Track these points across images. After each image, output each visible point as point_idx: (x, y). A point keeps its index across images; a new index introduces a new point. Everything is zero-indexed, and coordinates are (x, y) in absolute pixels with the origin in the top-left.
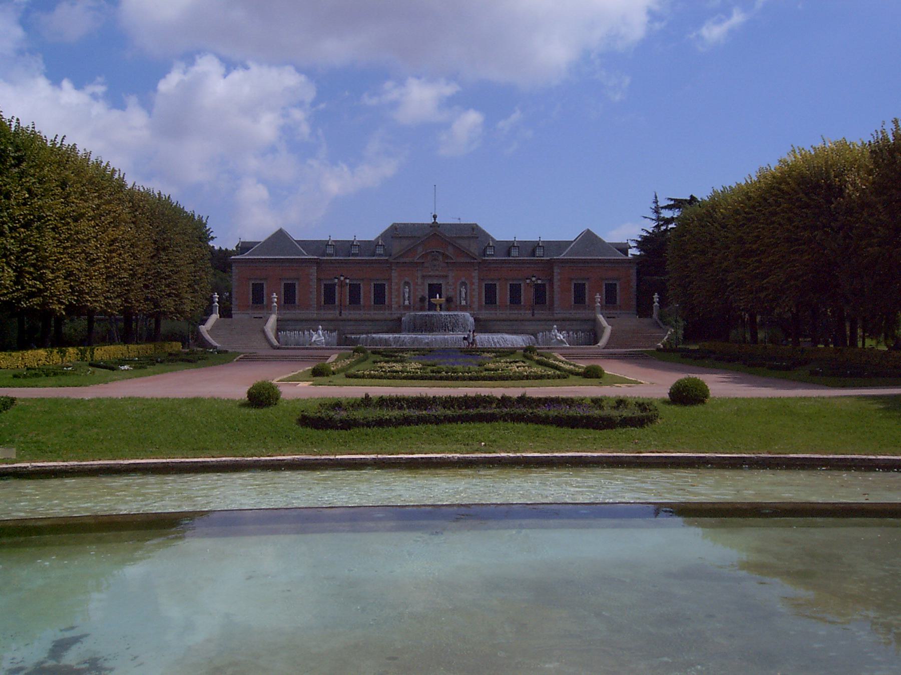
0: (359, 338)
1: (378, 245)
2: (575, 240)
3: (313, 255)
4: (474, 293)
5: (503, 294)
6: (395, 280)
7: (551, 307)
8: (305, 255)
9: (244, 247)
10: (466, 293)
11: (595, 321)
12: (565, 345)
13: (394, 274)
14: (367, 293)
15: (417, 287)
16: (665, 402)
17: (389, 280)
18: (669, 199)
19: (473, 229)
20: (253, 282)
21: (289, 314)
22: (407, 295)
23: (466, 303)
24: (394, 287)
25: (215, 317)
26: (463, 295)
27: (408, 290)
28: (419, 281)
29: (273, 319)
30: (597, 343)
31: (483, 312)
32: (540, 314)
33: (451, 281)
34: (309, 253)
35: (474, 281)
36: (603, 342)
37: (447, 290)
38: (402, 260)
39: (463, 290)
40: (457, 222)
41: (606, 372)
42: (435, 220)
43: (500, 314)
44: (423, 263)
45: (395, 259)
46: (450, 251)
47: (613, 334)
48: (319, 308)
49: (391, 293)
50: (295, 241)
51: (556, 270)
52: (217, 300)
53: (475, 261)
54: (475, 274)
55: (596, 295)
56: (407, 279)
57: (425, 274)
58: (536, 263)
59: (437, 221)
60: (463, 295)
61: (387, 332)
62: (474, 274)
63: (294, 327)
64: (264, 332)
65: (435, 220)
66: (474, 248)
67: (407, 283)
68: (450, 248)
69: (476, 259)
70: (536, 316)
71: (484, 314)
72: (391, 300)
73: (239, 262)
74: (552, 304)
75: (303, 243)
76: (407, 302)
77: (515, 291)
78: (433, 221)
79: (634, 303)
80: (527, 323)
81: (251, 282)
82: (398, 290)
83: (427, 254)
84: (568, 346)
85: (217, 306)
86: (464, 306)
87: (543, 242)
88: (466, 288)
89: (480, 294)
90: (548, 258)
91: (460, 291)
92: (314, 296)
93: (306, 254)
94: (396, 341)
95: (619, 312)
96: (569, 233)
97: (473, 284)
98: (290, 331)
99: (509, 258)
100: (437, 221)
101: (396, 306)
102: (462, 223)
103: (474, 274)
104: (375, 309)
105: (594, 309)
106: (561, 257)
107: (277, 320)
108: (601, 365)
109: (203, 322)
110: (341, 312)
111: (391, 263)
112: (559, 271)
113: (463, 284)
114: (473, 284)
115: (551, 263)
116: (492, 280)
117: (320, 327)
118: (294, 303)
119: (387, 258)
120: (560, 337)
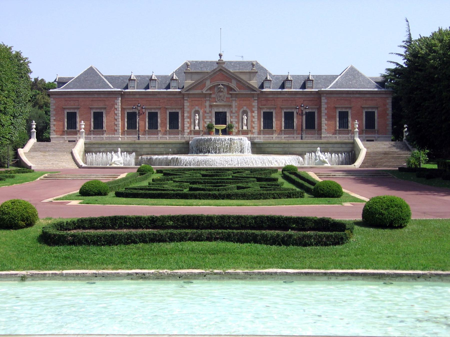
0: (151, 158)
1: (172, 79)
2: (340, 75)
3: (118, 88)
6: (187, 109)
8: (111, 88)
9: (61, 82)
10: (247, 120)
11: (354, 144)
12: (326, 165)
13: (187, 104)
15: (206, 115)
16: (358, 223)
17: (183, 109)
19: (253, 65)
21: (94, 138)
22: (197, 122)
23: (247, 128)
25: (33, 141)
26: (245, 122)
27: (197, 117)
28: (208, 110)
29: (81, 143)
30: (354, 163)
32: (309, 138)
36: (358, 164)
38: (191, 92)
39: (245, 117)
40: (240, 59)
41: (344, 190)
42: (221, 58)
43: (275, 138)
44: (211, 94)
46: (233, 85)
47: (367, 154)
48: (281, 132)
51: (324, 100)
52: (357, 126)
53: (255, 92)
54: (255, 104)
55: (33, 122)
59: (222, 59)
60: (245, 122)
62: (254, 104)
63: (99, 149)
64: (72, 153)
65: (221, 58)
66: (255, 83)
68: (234, 82)
69: (256, 91)
70: (305, 141)
71: (261, 139)
73: (71, 94)
74: (320, 129)
75: (112, 79)
76: (197, 128)
77: (153, 117)
79: (390, 128)
80: (297, 146)
83: (214, 87)
85: (34, 132)
86: (245, 130)
87: (293, 76)
88: (247, 116)
90: (317, 90)
91: (242, 119)
93: (112, 87)
95: (376, 135)
98: (96, 153)
100: (222, 59)
101: (189, 131)
103: (254, 104)
105: (353, 133)
106: (328, 89)
107: (85, 144)
108: (27, 199)
109: (23, 146)
110: (139, 137)
111: (183, 95)
112: (326, 101)
115: (319, 94)
116: (270, 108)
117: (119, 149)
119: (180, 90)
120: (322, 157)
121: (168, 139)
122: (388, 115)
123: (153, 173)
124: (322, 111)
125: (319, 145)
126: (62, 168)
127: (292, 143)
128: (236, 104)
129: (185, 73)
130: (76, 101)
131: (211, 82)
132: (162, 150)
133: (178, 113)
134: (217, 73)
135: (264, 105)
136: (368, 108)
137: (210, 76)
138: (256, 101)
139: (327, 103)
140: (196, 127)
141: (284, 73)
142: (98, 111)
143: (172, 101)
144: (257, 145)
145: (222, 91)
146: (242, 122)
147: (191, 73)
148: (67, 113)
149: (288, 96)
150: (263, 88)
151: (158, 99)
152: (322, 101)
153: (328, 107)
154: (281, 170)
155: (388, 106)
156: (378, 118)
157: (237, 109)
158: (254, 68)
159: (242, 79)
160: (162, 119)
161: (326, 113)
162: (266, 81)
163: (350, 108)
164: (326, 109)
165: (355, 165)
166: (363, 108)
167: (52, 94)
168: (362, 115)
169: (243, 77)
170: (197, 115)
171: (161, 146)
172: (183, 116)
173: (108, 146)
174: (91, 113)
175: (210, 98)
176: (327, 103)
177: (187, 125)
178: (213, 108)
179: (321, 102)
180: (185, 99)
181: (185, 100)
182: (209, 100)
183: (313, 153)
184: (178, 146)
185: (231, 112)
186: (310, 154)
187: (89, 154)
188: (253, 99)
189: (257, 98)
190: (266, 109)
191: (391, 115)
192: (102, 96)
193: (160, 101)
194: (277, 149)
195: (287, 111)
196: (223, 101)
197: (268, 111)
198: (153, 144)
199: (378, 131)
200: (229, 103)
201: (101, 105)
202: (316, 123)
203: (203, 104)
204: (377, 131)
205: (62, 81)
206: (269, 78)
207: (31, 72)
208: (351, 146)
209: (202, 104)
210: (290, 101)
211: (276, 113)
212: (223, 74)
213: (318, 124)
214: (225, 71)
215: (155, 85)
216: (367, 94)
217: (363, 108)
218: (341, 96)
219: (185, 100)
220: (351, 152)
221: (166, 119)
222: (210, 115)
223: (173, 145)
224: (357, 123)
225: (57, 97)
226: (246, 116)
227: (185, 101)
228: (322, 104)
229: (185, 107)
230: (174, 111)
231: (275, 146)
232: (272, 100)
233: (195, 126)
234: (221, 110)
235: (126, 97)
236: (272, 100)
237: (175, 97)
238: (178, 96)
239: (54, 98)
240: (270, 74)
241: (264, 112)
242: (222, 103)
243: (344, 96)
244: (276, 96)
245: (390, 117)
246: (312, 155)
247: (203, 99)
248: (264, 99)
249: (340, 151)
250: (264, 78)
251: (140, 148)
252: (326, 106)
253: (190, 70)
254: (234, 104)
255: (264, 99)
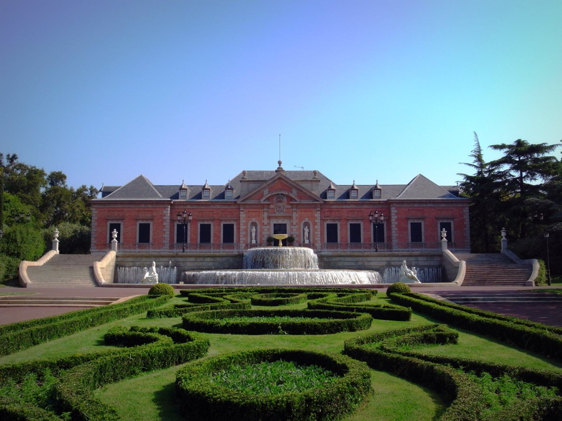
4: (316, 233)
5: (344, 233)
6: (242, 221)
7: (389, 247)
10: (309, 233)
12: (416, 283)
13: (243, 215)
14: (217, 232)
15: (264, 227)
17: (238, 220)
18: (496, 147)
20: (441, 221)
23: (309, 242)
24: (242, 227)
26: (306, 234)
28: (266, 221)
31: (325, 250)
33: (295, 221)
34: (164, 197)
35: (316, 221)
37: (292, 229)
39: (307, 230)
40: (301, 170)
42: (280, 165)
44: (269, 204)
45: (242, 201)
49: (239, 232)
50: (153, 186)
51: (394, 211)
54: (318, 215)
56: (254, 220)
57: (271, 215)
58: (355, 204)
59: (281, 166)
60: (306, 234)
61: (217, 269)
65: (280, 165)
67: (254, 224)
68: (294, 191)
71: (326, 252)
72: (240, 239)
75: (161, 188)
77: (355, 231)
78: (278, 166)
79: (468, 240)
81: (410, 222)
82: (246, 230)
84: (420, 283)
88: (309, 228)
89: (322, 234)
92: (167, 235)
94: (241, 278)
96: (404, 179)
97: (315, 224)
99: (371, 200)
100: (281, 166)
102: (304, 170)
104: (351, 248)
106: (398, 198)
111: (239, 205)
112: (396, 211)
113: (306, 224)
114: (315, 224)
115: (389, 203)
116: (334, 220)
117: (154, 263)
118: (337, 241)
121: (222, 252)
122: (465, 226)
123: (171, 297)
124: (393, 223)
125: (406, 258)
126: (73, 286)
127: (368, 256)
128: (297, 215)
129: (241, 181)
130: (121, 212)
131: (269, 192)
132: (211, 264)
133: (233, 225)
134: (276, 182)
135: (328, 217)
136: (443, 219)
137: (268, 185)
138: (319, 212)
139: (397, 214)
140: (253, 241)
141: (348, 182)
142: (145, 222)
143: (227, 213)
144: (325, 258)
145: (282, 201)
146: (304, 235)
147: (248, 181)
148: (110, 224)
149: (354, 207)
150: (326, 198)
151: (211, 210)
152: (392, 211)
153: (398, 218)
154: (385, 290)
155: (465, 217)
156: (454, 230)
157: (297, 221)
158: (316, 177)
159: (303, 188)
160: (216, 232)
161: (396, 225)
162: (329, 191)
163: (423, 219)
164: (396, 220)
165: (457, 283)
166: (437, 219)
167: (94, 204)
168: (437, 226)
169: (304, 185)
170: (254, 227)
171: (208, 259)
172: (239, 229)
173: (144, 259)
174: (136, 225)
175: (268, 208)
176: (397, 214)
177: (242, 239)
178: (272, 219)
179: (390, 212)
180: (241, 209)
181: (241, 211)
182: (268, 211)
183: (393, 268)
184: (232, 260)
185: (292, 224)
186: (390, 269)
187: (130, 268)
188: (315, 210)
189: (319, 209)
190: (329, 221)
191: (468, 226)
192: (150, 206)
193: (213, 212)
194: (349, 264)
195: (353, 223)
196: (283, 212)
197: (332, 223)
198: (200, 257)
199: (455, 244)
200: (289, 215)
201: (149, 215)
202: (385, 236)
203: (260, 215)
204: (453, 245)
205: (106, 190)
206: (333, 187)
207: (86, 186)
208: (438, 259)
209: (259, 216)
210: (356, 212)
211: (340, 225)
212: (282, 183)
213: (387, 237)
214: (285, 179)
215: (208, 195)
216: (441, 203)
217: (437, 219)
218: (411, 205)
219: (241, 211)
220: (440, 266)
221: (220, 232)
222: (268, 227)
223: (224, 259)
224: (444, 231)
225: (99, 206)
226: (308, 228)
227: (241, 213)
228: (392, 214)
229: (241, 218)
230: (228, 223)
231: (347, 259)
232: (336, 211)
233: (251, 239)
234: (280, 222)
235: (176, 207)
236: (336, 211)
237: (230, 207)
238: (233, 207)
239: (96, 208)
240: (334, 184)
241: (327, 224)
242: (282, 214)
243: (416, 205)
244: (340, 207)
245: (467, 229)
246: (392, 270)
247: (260, 210)
248: (327, 210)
249: (426, 265)
250: (327, 188)
251: (183, 262)
252: (396, 217)
253: (247, 178)
254: (295, 215)
255: (327, 210)
